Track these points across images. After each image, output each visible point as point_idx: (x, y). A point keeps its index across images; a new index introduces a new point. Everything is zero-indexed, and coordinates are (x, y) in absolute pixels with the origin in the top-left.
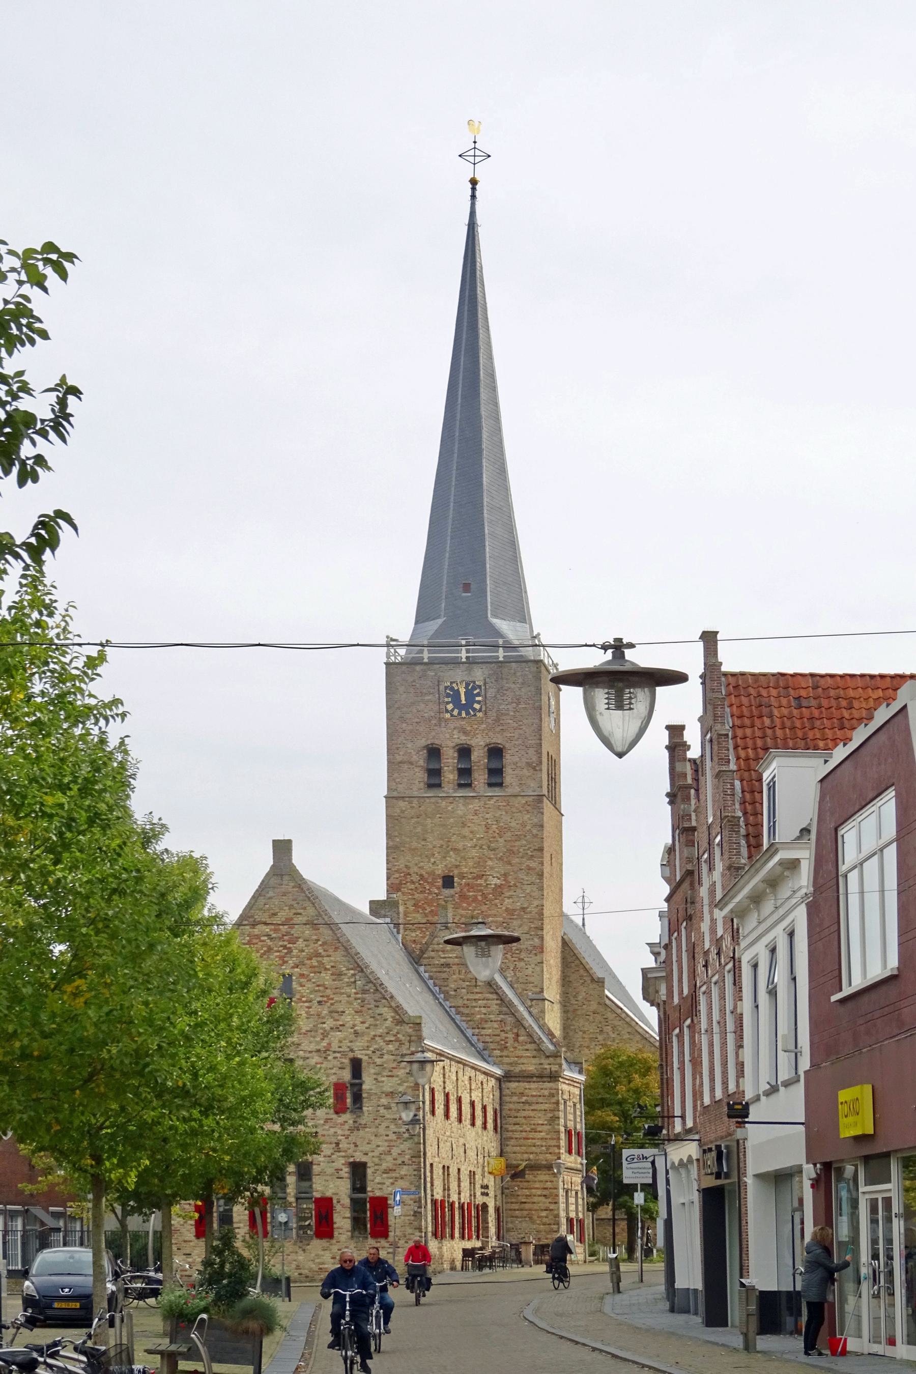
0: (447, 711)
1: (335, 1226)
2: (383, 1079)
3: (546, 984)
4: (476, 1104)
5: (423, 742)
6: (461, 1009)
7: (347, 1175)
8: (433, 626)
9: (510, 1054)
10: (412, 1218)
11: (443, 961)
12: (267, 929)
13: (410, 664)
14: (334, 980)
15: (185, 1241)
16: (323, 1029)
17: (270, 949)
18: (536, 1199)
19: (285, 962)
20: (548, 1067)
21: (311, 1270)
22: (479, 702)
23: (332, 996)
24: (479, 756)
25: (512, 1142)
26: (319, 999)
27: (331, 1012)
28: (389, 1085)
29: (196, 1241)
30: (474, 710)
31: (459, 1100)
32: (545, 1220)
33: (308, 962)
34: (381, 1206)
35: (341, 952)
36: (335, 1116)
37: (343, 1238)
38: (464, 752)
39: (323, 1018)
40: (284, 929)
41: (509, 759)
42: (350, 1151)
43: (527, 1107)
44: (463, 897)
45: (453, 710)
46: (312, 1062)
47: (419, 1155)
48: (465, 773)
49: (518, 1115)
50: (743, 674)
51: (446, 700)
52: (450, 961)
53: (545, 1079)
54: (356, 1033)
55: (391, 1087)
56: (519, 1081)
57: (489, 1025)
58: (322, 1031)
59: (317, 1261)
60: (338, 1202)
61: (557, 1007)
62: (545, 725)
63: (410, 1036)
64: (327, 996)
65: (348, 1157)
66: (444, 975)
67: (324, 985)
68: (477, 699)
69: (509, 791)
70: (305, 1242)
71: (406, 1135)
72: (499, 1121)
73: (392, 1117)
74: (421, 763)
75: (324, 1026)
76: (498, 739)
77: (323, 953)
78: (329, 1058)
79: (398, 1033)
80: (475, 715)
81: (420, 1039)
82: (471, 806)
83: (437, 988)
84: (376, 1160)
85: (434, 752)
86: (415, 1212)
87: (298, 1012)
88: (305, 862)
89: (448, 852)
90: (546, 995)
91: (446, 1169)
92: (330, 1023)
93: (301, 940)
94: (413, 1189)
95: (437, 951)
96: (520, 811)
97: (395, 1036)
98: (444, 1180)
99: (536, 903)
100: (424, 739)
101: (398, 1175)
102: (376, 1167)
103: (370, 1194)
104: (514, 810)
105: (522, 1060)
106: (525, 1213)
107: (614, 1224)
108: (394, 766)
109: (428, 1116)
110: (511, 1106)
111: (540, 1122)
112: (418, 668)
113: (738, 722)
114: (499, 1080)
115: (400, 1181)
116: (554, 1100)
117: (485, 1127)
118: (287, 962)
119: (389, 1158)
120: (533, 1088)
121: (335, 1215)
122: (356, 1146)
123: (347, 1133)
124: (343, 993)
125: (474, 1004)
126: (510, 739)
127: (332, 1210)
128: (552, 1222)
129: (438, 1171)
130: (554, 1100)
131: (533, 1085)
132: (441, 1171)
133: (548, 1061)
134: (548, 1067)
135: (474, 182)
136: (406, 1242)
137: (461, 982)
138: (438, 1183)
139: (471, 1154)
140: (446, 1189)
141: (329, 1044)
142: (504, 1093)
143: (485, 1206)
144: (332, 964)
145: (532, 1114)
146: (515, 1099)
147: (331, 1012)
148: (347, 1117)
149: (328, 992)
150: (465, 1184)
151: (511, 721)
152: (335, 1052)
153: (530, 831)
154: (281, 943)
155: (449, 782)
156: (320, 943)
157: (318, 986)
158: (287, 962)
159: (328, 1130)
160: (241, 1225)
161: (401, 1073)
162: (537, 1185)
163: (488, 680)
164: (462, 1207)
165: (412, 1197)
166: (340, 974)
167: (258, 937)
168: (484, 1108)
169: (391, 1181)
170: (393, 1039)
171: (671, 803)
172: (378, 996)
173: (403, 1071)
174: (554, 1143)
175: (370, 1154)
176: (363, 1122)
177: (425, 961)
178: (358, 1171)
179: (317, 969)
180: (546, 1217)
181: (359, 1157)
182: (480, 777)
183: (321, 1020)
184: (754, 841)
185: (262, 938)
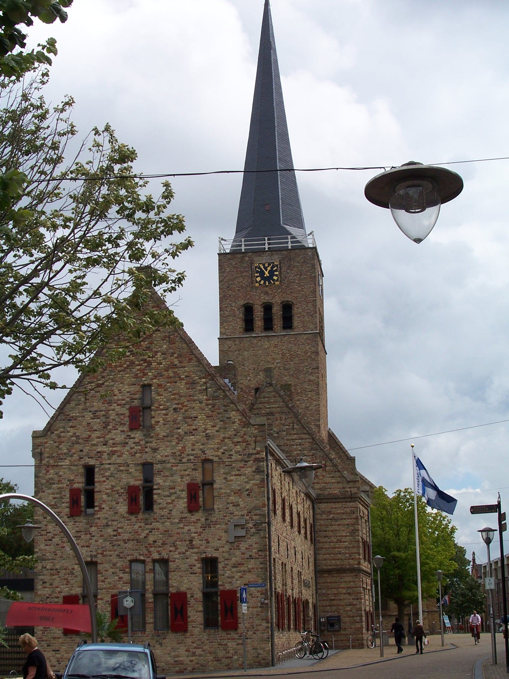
0: (257, 282)
1: (189, 620)
2: (232, 478)
5: (242, 302)
7: (199, 570)
10: (260, 609)
11: (268, 410)
13: (233, 253)
14: (188, 389)
15: (54, 638)
18: (342, 597)
19: (145, 374)
21: (167, 663)
22: (276, 275)
23: (186, 403)
24: (277, 311)
27: (185, 418)
28: (236, 482)
29: (64, 638)
30: (274, 280)
32: (349, 613)
34: (231, 600)
35: (194, 362)
36: (188, 515)
37: (196, 631)
38: (268, 308)
39: (179, 423)
41: (296, 311)
42: (202, 548)
45: (260, 281)
48: (268, 325)
51: (256, 275)
52: (274, 410)
53: (347, 500)
54: (208, 436)
55: (239, 485)
56: (327, 503)
59: (173, 654)
63: (256, 437)
64: (182, 404)
68: (275, 273)
71: (253, 530)
73: (240, 513)
75: (179, 431)
77: (178, 365)
79: (245, 434)
80: (274, 283)
82: (273, 342)
84: (226, 555)
85: (248, 310)
86: (262, 603)
87: (156, 419)
89: (258, 373)
91: (284, 565)
93: (159, 354)
94: (260, 581)
95: (264, 403)
96: (304, 344)
97: (242, 437)
98: (283, 575)
99: (315, 403)
100: (242, 300)
101: (246, 569)
102: (226, 562)
103: (221, 588)
104: (300, 343)
105: (329, 486)
106: (334, 608)
110: (322, 522)
112: (239, 256)
115: (247, 574)
116: (354, 516)
118: (147, 374)
119: (238, 553)
120: (338, 508)
121: (189, 609)
123: (200, 530)
125: (292, 443)
126: (296, 298)
127: (186, 604)
128: (355, 615)
129: (279, 567)
130: (354, 516)
132: (281, 566)
134: (348, 490)
136: (254, 633)
137: (282, 426)
140: (284, 584)
141: (184, 447)
142: (316, 512)
143: (307, 602)
144: (186, 374)
145: (337, 528)
146: (324, 516)
147: (185, 418)
148: (199, 515)
149: (183, 399)
151: (297, 287)
152: (188, 455)
153: (310, 356)
154: (142, 357)
156: (176, 355)
157: (174, 394)
158: (147, 374)
161: (248, 471)
162: (343, 585)
163: (282, 261)
165: (259, 589)
166: (194, 383)
169: (240, 574)
170: (240, 440)
172: (227, 401)
174: (355, 550)
176: (214, 519)
178: (210, 565)
180: (351, 611)
181: (211, 553)
183: (175, 426)
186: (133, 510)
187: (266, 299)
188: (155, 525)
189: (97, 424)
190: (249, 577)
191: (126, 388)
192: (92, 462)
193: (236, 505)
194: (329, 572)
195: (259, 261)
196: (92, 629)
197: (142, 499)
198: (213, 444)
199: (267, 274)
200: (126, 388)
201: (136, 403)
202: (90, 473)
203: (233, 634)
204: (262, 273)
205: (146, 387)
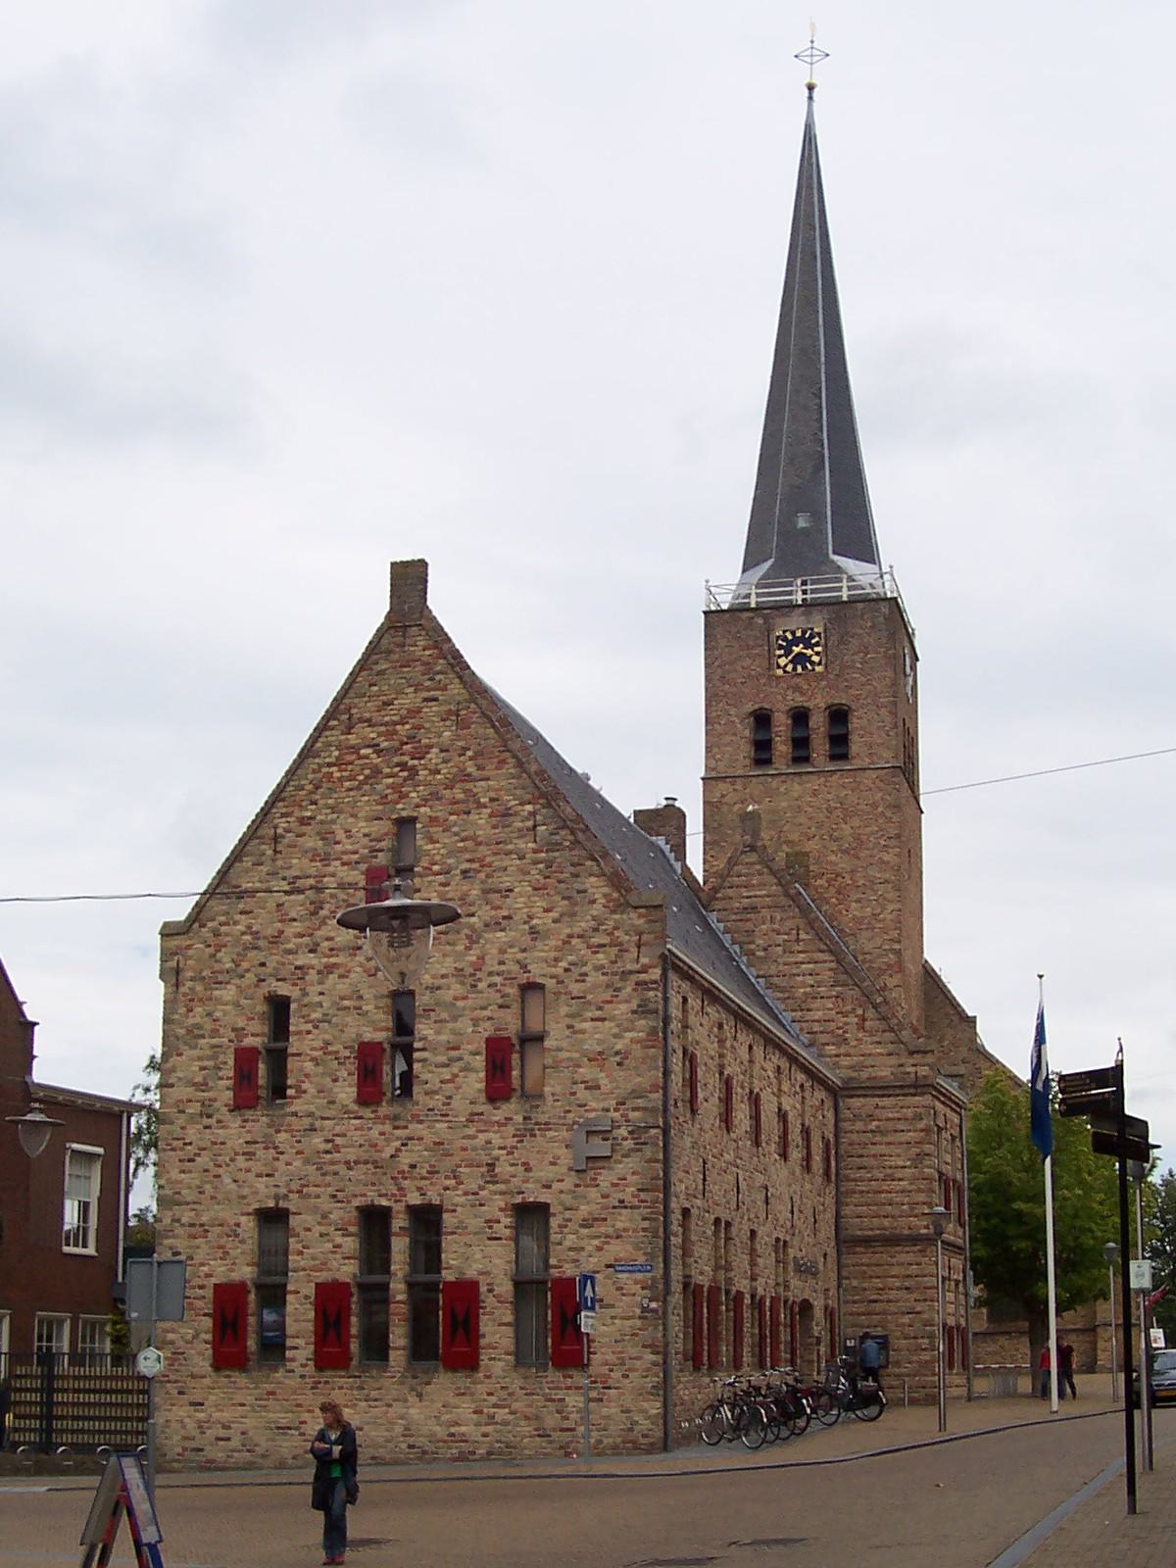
0: (779, 667)
1: (483, 1342)
4: (790, 1118)
5: (750, 707)
6: (775, 980)
9: (852, 1051)
10: (638, 1323)
12: (372, 734)
14: (495, 827)
15: (193, 1376)
16: (472, 927)
17: (376, 772)
19: (403, 796)
20: (912, 1069)
24: (818, 722)
25: (856, 1198)
26: (466, 866)
27: (486, 892)
31: (755, 1100)
33: (447, 793)
37: (498, 1368)
38: (800, 717)
40: (403, 730)
41: (855, 723)
43: (878, 1138)
46: (447, 995)
48: (801, 747)
49: (864, 1152)
51: (778, 652)
54: (534, 932)
55: (600, 1042)
57: (818, 1003)
58: (466, 931)
59: (446, 1417)
60: (490, 1291)
64: (480, 860)
65: (511, 1193)
66: (749, 926)
67: (473, 838)
69: (856, 764)
70: (423, 1378)
72: (833, 1163)
74: (747, 733)
75: (473, 920)
78: (481, 986)
79: (616, 928)
83: (737, 948)
84: (567, 1199)
94: (641, 1260)
101: (611, 1230)
105: (869, 1061)
107: (1083, 1331)
110: (854, 1137)
111: (901, 1163)
112: (746, 615)
121: (483, 1319)
122: (528, 1169)
124: (508, 853)
126: (857, 697)
131: (886, 1102)
133: (912, 1061)
134: (912, 1069)
135: (811, 88)
138: (702, 1252)
139: (782, 1209)
140: (723, 1265)
141: (482, 958)
143: (806, 1307)
144: (492, 794)
146: (859, 1125)
152: (490, 974)
154: (396, 760)
155: (780, 756)
156: (469, 753)
159: (474, 1137)
160: (300, 1342)
162: (895, 1271)
165: (639, 1276)
166: (507, 814)
167: (355, 749)
168: (806, 1132)
169: (596, 1242)
173: (624, 1007)
175: (556, 1186)
177: (718, 905)
178: (531, 1216)
179: (462, 807)
184: (960, 1248)
185: (363, 752)
186: (369, 1091)
188: (415, 1128)
189: (297, 905)
191: (362, 827)
192: (283, 989)
197: (383, 1072)
198: (545, 949)
200: (362, 827)
201: (382, 859)
202: (279, 1010)
203: (579, 1378)
205: (405, 824)
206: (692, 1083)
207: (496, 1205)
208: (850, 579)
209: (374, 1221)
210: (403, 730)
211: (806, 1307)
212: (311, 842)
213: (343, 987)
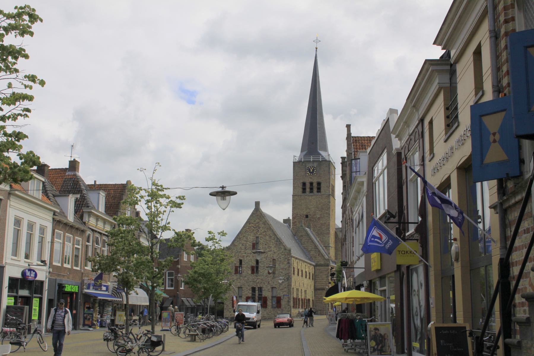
3: (330, 242)
5: (302, 181)
8: (304, 153)
13: (300, 162)
24: (315, 185)
28: (282, 266)
31: (302, 271)
38: (311, 184)
40: (257, 225)
41: (322, 185)
44: (310, 220)
47: (289, 285)
48: (311, 189)
50: (358, 137)
61: (333, 248)
62: (331, 177)
76: (319, 180)
81: (290, 254)
85: (304, 184)
88: (265, 209)
90: (330, 245)
92: (268, 250)
108: (294, 188)
109: (292, 275)
113: (356, 150)
114: (315, 266)
117: (310, 278)
135: (316, 48)
139: (305, 285)
140: (297, 295)
143: (309, 300)
150: (303, 293)
164: (302, 300)
168: (309, 273)
171: (342, 179)
182: (315, 190)
186: (253, 272)
187: (311, 180)
188: (259, 277)
189: (243, 247)
190: (285, 293)
191: (252, 237)
192: (241, 258)
193: (282, 272)
194: (319, 289)
195: (309, 165)
196: (51, 210)
197: (255, 269)
198: (276, 255)
199: (311, 171)
200: (252, 237)
201: (254, 242)
202: (241, 261)
203: (280, 309)
204: (310, 170)
205: (257, 237)
206: (294, 271)
207: (269, 287)
208: (322, 156)
209: (253, 289)
210: (257, 225)
211: (309, 300)
212: (245, 239)
213: (249, 258)
